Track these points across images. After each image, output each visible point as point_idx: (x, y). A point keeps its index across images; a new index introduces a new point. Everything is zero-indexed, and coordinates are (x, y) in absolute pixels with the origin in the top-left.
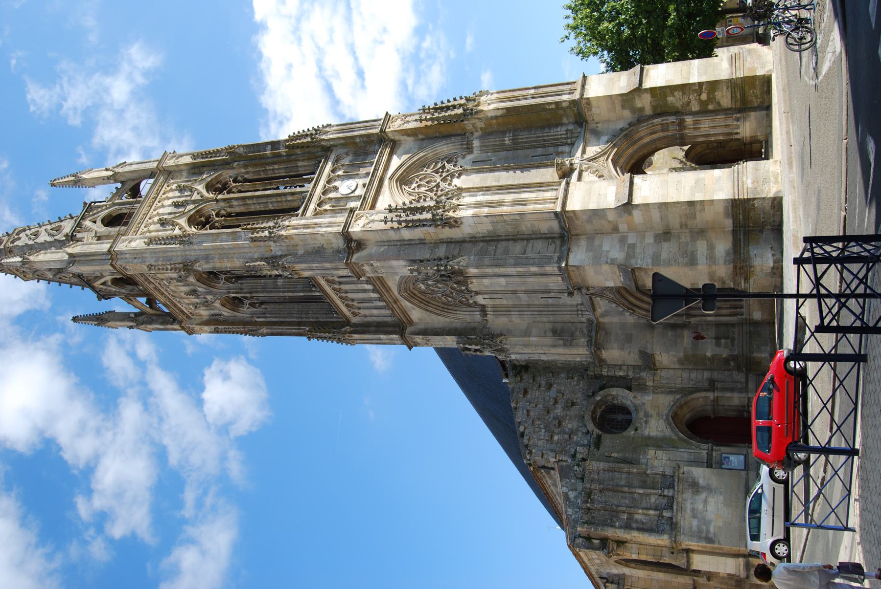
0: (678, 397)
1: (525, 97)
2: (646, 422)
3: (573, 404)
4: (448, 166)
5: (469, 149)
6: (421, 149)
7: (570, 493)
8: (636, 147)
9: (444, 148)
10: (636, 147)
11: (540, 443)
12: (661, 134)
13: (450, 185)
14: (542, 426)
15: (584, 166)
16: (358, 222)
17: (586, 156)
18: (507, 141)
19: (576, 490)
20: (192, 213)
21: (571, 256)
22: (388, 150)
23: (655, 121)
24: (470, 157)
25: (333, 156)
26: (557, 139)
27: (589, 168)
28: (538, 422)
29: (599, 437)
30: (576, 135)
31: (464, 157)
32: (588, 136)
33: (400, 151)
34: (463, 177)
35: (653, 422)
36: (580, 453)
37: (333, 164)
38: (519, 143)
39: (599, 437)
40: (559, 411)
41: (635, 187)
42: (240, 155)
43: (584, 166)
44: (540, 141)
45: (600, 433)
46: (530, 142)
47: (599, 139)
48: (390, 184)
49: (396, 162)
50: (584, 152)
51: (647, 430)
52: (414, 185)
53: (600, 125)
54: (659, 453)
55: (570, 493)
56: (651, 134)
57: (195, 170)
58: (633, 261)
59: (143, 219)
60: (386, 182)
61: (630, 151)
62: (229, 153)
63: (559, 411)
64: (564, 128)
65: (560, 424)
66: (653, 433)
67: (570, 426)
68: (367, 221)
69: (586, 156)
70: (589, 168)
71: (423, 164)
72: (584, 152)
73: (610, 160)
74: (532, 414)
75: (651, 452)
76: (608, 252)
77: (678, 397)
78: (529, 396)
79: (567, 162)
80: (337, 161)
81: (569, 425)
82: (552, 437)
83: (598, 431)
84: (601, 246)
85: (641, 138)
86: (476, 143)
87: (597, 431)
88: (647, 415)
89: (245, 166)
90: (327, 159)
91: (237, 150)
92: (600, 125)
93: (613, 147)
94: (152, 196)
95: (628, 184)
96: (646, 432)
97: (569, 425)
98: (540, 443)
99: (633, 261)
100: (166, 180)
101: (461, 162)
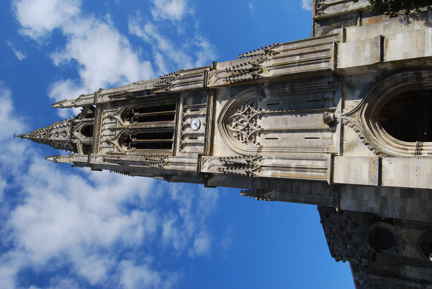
0: (424, 231)
1: (293, 64)
2: (404, 247)
3: (357, 226)
4: (252, 110)
5: (264, 96)
6: (232, 96)
7: (360, 281)
8: (383, 97)
9: (247, 95)
10: (383, 97)
11: (340, 249)
12: (403, 84)
13: (255, 125)
14: (340, 239)
15: (345, 121)
16: (205, 164)
17: (346, 111)
18: (287, 90)
19: (363, 280)
20: (119, 136)
21: (342, 201)
22: (212, 98)
23: (397, 75)
24: (265, 100)
25: (182, 99)
26: (323, 89)
27: (348, 122)
28: (337, 236)
29: (374, 254)
30: (336, 86)
31: (261, 101)
32: (345, 89)
33: (220, 96)
34: (263, 118)
35: (408, 248)
36: (364, 263)
37: (183, 105)
38: (296, 91)
39: (374, 254)
40: (349, 229)
41: (383, 169)
42: (132, 97)
43: (345, 121)
44: (311, 90)
45: (375, 251)
46: (304, 91)
47: (353, 93)
48: (218, 125)
49: (219, 107)
50: (343, 106)
51: (404, 253)
52: (234, 124)
53: (353, 78)
54: (413, 268)
55: (360, 281)
56: (394, 85)
57: (114, 104)
58: (385, 212)
59: (98, 139)
60: (216, 124)
61: (379, 101)
62: (126, 96)
63: (349, 229)
64: (326, 81)
65: (350, 239)
66: (408, 255)
67: (356, 239)
68: (210, 165)
69: (346, 111)
70: (348, 122)
71: (235, 108)
72: (343, 106)
73: (363, 116)
74: (333, 230)
75: (408, 268)
76: (367, 201)
77: (424, 231)
78: (330, 218)
79: (332, 117)
80: (184, 104)
81: (356, 239)
82: (346, 246)
83: (373, 250)
84: (362, 195)
85: (386, 90)
86: (267, 92)
87: (372, 250)
88: (404, 242)
89: (137, 103)
90: (179, 104)
91: (129, 95)
92: (353, 78)
93: (364, 103)
94: (96, 141)
95: (377, 167)
96: (404, 254)
97: (356, 239)
98: (340, 249)
99: (385, 212)
100: (102, 111)
101: (260, 104)
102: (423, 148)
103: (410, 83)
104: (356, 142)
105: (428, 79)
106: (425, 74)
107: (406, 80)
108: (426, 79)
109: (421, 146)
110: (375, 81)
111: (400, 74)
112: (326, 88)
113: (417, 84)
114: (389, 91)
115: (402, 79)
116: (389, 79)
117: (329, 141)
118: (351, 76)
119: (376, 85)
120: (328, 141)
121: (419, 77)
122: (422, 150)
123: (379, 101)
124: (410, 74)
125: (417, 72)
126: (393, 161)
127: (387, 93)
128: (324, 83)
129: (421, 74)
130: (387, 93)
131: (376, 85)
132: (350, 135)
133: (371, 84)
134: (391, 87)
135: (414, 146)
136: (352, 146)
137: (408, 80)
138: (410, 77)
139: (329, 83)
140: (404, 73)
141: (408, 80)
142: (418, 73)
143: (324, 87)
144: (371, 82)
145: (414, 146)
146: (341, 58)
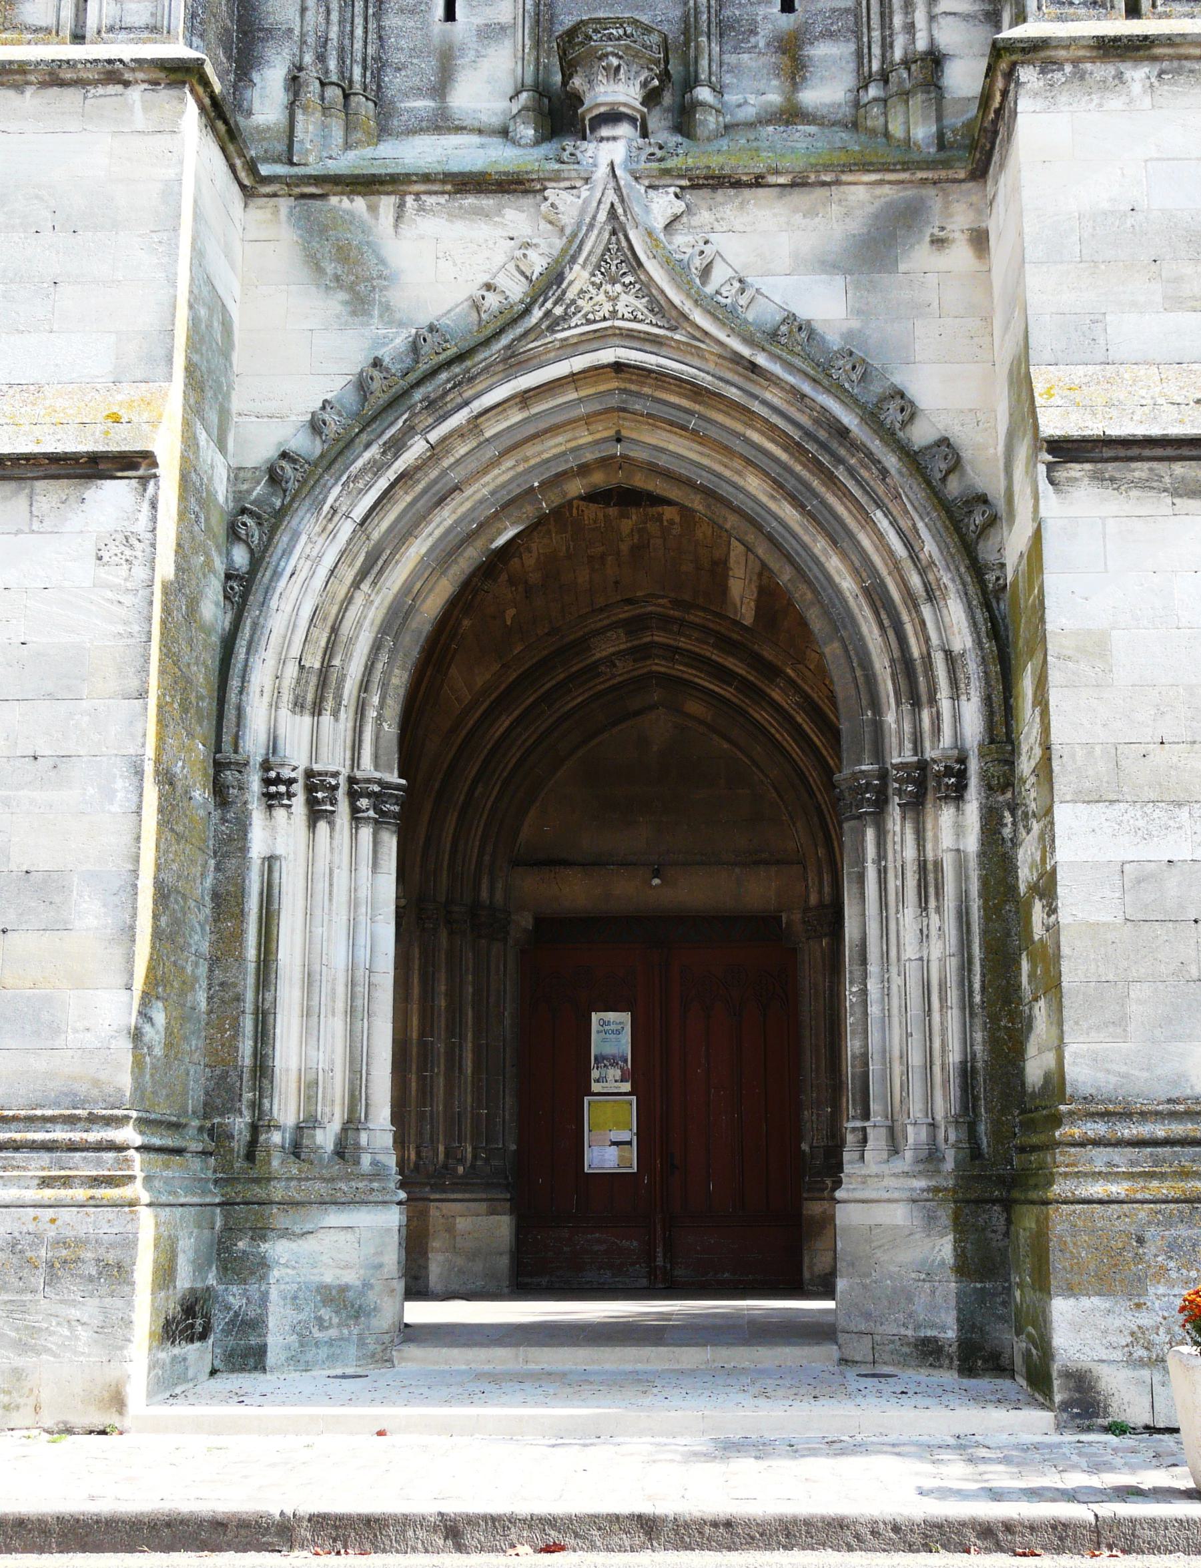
41: (49, 494)
53: (960, 254)
56: (877, 596)
61: (754, 484)
85: (838, 536)
102: (366, 833)
103: (890, 718)
104: (387, 308)
105: (910, 853)
106: (956, 830)
107: (915, 693)
108: (910, 837)
109: (355, 810)
110: (921, 435)
111: (962, 638)
112: (887, 45)
113: (883, 775)
114: (834, 564)
115: (927, 659)
116: (930, 547)
117: (423, 104)
118: (980, 240)
119: (876, 446)
120: (418, 92)
121: (934, 783)
122: (315, 814)
123: (754, 484)
124: (964, 720)
125: (974, 766)
126: (116, 575)
127: (820, 546)
128: (932, 18)
129: (958, 794)
130: (820, 546)
131: (876, 446)
132: (448, 263)
133: (890, 410)
134: (863, 568)
135: (355, 761)
136: (351, 277)
137: (916, 704)
138: (937, 719)
139: (935, 60)
140: (972, 667)
141: (916, 704)
142: (962, 775)
143: (898, 21)
144: (910, 411)
145: (355, 761)
146: (1115, 103)
